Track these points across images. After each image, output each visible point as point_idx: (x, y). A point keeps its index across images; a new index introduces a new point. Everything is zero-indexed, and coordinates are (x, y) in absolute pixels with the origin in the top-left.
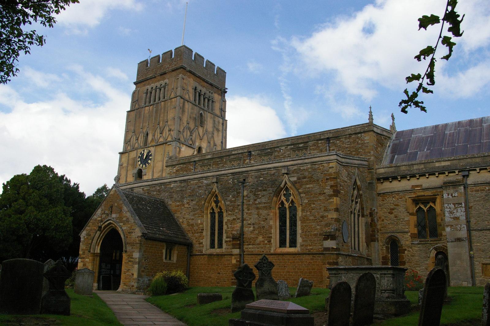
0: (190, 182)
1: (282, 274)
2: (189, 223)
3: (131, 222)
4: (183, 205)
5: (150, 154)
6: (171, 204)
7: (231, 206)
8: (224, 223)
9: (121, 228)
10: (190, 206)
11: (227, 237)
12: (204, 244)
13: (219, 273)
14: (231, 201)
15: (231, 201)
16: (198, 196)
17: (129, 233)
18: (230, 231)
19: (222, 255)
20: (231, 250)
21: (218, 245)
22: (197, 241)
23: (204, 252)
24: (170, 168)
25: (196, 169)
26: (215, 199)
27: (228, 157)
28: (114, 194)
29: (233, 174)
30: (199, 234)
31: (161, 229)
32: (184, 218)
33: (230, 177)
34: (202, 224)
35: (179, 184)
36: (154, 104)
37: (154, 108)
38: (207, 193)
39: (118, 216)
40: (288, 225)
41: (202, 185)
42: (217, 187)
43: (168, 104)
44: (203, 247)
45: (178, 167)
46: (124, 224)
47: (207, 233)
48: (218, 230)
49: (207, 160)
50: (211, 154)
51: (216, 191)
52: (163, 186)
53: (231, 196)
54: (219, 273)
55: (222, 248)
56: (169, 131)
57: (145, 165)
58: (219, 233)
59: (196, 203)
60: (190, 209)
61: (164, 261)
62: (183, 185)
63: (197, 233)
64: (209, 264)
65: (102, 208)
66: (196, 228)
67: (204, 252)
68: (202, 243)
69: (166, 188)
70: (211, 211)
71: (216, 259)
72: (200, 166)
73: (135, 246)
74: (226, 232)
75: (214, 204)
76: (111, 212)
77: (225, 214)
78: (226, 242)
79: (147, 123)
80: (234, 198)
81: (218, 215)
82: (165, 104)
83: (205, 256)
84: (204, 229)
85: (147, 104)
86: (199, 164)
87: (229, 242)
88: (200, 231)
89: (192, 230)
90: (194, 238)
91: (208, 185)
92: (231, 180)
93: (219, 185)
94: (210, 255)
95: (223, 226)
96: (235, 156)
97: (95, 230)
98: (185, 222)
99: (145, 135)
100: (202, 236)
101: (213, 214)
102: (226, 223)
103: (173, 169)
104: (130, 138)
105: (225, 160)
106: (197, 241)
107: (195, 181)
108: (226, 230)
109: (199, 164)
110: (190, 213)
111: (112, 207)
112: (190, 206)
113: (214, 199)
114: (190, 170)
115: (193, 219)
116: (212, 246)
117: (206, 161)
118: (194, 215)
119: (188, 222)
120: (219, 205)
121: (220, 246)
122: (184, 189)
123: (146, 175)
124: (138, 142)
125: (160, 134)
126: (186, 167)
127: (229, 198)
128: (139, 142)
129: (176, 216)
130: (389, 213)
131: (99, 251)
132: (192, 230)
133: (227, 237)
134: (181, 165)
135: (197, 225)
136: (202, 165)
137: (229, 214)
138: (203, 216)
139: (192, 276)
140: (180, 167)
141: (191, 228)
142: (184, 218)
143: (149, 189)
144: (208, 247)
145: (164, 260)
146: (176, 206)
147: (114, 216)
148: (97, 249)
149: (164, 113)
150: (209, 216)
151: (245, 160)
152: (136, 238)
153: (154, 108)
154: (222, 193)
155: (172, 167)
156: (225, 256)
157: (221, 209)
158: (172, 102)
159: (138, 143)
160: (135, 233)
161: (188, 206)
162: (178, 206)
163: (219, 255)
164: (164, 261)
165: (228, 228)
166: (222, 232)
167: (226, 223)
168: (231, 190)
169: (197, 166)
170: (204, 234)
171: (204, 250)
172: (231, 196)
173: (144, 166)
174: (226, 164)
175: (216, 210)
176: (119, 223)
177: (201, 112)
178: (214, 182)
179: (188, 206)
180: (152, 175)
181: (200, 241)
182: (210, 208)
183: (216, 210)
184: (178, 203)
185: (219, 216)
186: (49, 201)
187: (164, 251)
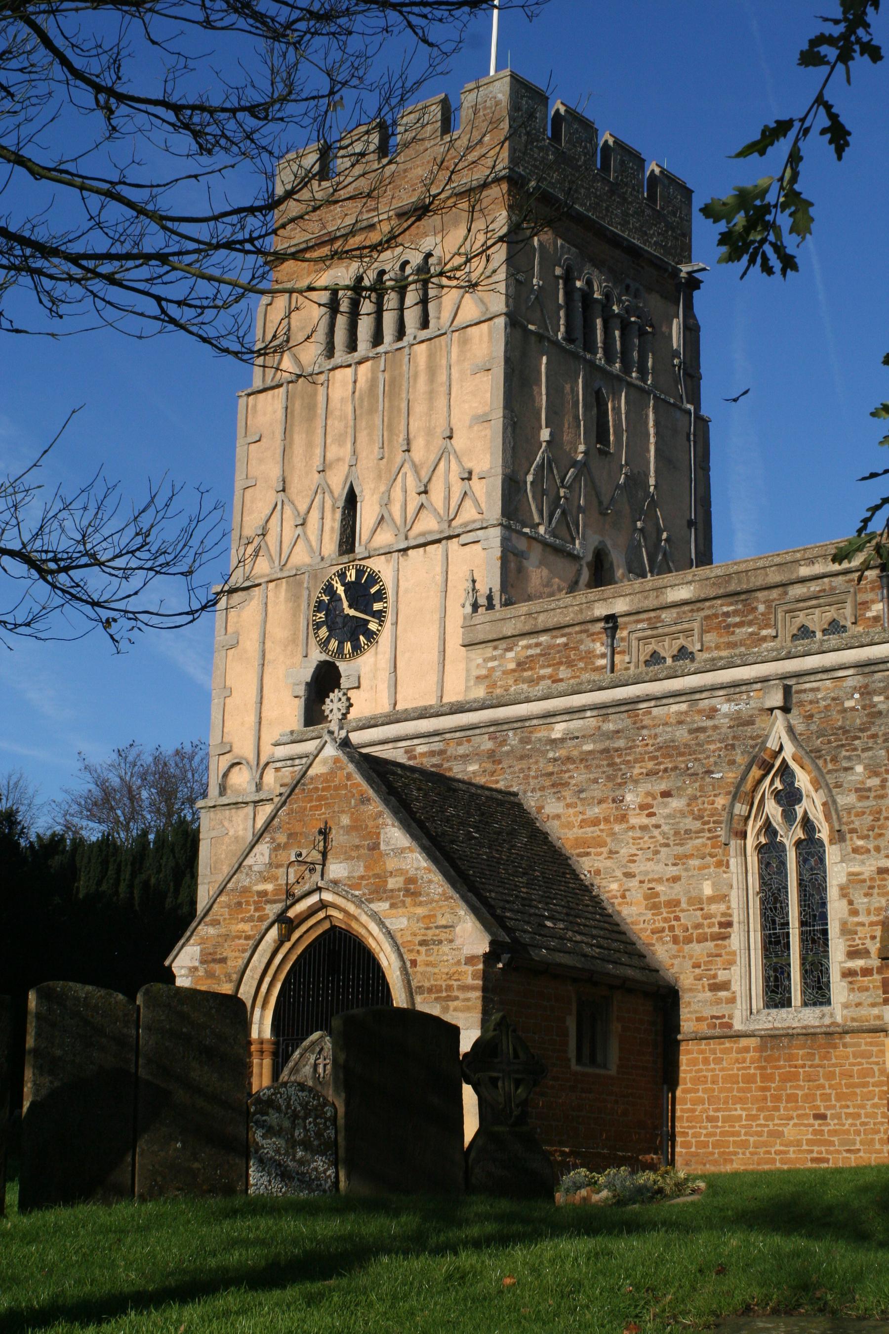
0: (650, 713)
2: (657, 895)
4: (623, 818)
5: (373, 591)
6: (558, 817)
8: (833, 893)
10: (653, 820)
11: (853, 954)
12: (735, 987)
13: (823, 1117)
14: (862, 792)
15: (862, 792)
17: (423, 943)
18: (862, 924)
19: (831, 1036)
20: (876, 1011)
21: (803, 993)
23: (738, 1026)
24: (489, 652)
25: (622, 652)
26: (778, 785)
27: (775, 594)
28: (332, 773)
29: (863, 666)
30: (710, 944)
32: (629, 875)
33: (850, 683)
34: (723, 898)
35: (593, 722)
36: (377, 357)
37: (381, 376)
38: (739, 759)
39: (361, 871)
40: (795, 984)
41: (710, 723)
42: (790, 730)
43: (449, 353)
44: (732, 1000)
45: (528, 647)
46: (393, 906)
47: (746, 942)
48: (803, 924)
49: (674, 611)
51: (781, 748)
52: (511, 734)
53: (859, 769)
54: (823, 1117)
55: (829, 1003)
58: (805, 938)
59: (689, 805)
60: (656, 832)
61: (574, 1067)
62: (610, 726)
63: (699, 942)
64: (765, 1078)
65: (273, 839)
66: (689, 917)
67: (738, 1026)
68: (725, 986)
69: (527, 743)
70: (763, 840)
71: (801, 1052)
72: (639, 640)
73: (456, 998)
74: (846, 931)
75: (773, 809)
76: (324, 854)
77: (832, 854)
78: (848, 974)
79: (349, 445)
81: (798, 855)
82: (431, 356)
83: (744, 1042)
84: (735, 919)
85: (340, 356)
86: (633, 627)
87: (864, 975)
88: (716, 929)
90: (688, 964)
91: (742, 722)
92: (857, 696)
95: (824, 904)
96: (814, 587)
97: (248, 938)
98: (637, 894)
100: (728, 954)
101: (770, 852)
102: (842, 888)
103: (502, 656)
104: (264, 517)
105: (761, 608)
106: (699, 978)
107: (674, 708)
108: (844, 924)
109: (633, 627)
110: (657, 852)
111: (324, 833)
112: (653, 820)
113: (772, 782)
115: (675, 879)
116: (776, 993)
117: (665, 615)
118: (680, 860)
121: (818, 992)
122: (621, 743)
123: (358, 687)
124: (305, 533)
125: (419, 494)
126: (566, 645)
127: (850, 779)
129: (586, 866)
130: (660, 1191)
131: (267, 1034)
132: (672, 929)
133: (853, 954)
134: (544, 638)
135: (697, 902)
136: (649, 633)
137: (856, 850)
138: (723, 864)
139: (685, 1134)
140: (537, 645)
141: (665, 920)
142: (629, 875)
143: (442, 752)
144: (758, 1002)
145: (573, 1061)
146: (583, 824)
147: (337, 869)
148: (261, 1023)
149: (431, 395)
150: (753, 860)
151: (866, 605)
152: (458, 963)
153: (381, 376)
154: (815, 754)
155: (495, 648)
156: (848, 1039)
158: (464, 342)
159: (308, 540)
160: (451, 941)
161: (646, 821)
162: (595, 822)
163: (814, 1034)
164: (574, 1067)
165: (854, 913)
166: (825, 932)
167: (842, 888)
168: (856, 742)
170: (736, 941)
171: (737, 1014)
172: (859, 769)
173: (348, 646)
175: (790, 836)
177: (596, 386)
178: (771, 710)
179: (646, 821)
180: (389, 687)
181: (715, 976)
182: (753, 826)
183: (790, 836)
184: (597, 810)
187: (571, 1024)
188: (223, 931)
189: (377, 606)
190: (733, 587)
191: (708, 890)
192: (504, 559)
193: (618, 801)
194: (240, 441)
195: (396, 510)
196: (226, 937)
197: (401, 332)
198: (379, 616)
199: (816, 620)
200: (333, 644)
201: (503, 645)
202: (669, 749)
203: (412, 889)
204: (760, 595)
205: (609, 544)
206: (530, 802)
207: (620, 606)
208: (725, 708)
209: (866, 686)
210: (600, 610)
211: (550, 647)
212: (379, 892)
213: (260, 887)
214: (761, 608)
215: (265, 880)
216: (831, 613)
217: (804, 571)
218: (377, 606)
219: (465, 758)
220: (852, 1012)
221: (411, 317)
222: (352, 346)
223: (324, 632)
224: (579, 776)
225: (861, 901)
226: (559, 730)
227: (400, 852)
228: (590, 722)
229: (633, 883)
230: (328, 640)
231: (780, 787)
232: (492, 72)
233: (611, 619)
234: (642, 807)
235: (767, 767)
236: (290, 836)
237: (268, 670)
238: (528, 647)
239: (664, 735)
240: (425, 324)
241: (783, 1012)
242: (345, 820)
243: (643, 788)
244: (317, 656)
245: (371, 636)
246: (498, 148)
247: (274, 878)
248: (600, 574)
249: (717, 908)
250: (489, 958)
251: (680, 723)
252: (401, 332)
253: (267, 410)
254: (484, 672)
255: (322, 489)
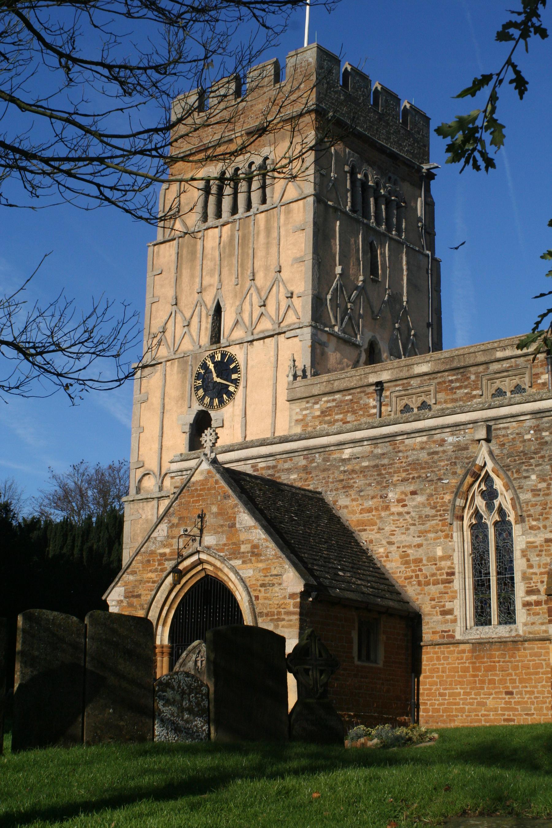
0: (404, 442)
1: (535, 701)
3: (266, 555)
4: (387, 508)
5: (231, 367)
6: (346, 507)
7: (536, 505)
9: (236, 573)
10: (406, 509)
11: (529, 592)
12: (457, 612)
13: (511, 693)
14: (535, 492)
15: (535, 492)
16: (430, 481)
17: (263, 585)
18: (535, 574)
19: (516, 643)
20: (544, 628)
21: (499, 616)
22: (434, 607)
23: (458, 637)
24: (304, 404)
25: (386, 405)
26: (483, 487)
27: (481, 368)
28: (206, 480)
29: (536, 414)
30: (441, 586)
31: (341, 573)
32: (390, 543)
33: (528, 424)
34: (449, 557)
35: (368, 448)
37: (236, 233)
38: (459, 471)
39: (224, 540)
42: (491, 453)
43: (279, 219)
44: (455, 621)
45: (328, 401)
46: (244, 562)
47: (463, 585)
48: (498, 573)
49: (419, 379)
50: (428, 362)
51: (485, 464)
52: (317, 455)
53: (534, 477)
54: (511, 693)
55: (515, 622)
56: (287, 297)
57: (212, 400)
58: (500, 582)
59: (428, 500)
61: (357, 662)
62: (379, 451)
63: (434, 584)
64: (475, 669)
66: (428, 569)
67: (458, 637)
68: (450, 612)
69: (327, 461)
70: (474, 521)
71: (497, 653)
72: (397, 397)
74: (526, 578)
75: (480, 502)
76: (201, 530)
77: (517, 530)
78: (527, 604)
79: (217, 276)
80: (544, 480)
81: (496, 531)
82: (268, 221)
83: (462, 647)
84: (457, 571)
85: (211, 221)
86: (393, 389)
87: (536, 605)
88: (445, 577)
89: (417, 576)
90: (428, 598)
91: (461, 448)
92: (532, 432)
93: (494, 446)
94: (479, 645)
95: (512, 561)
96: (506, 364)
98: (395, 555)
99: (212, 312)
100: (452, 592)
101: (478, 529)
102: (523, 551)
104: (164, 321)
105: (473, 377)
107: (419, 439)
108: (524, 574)
109: (393, 389)
110: (408, 529)
111: (201, 517)
112: (406, 509)
113: (479, 486)
114: (366, 407)
115: (419, 546)
116: (482, 616)
117: (413, 382)
119: (405, 555)
120: (496, 503)
121: (508, 615)
122: (385, 461)
123: (222, 427)
124: (189, 331)
125: (260, 306)
126: (351, 400)
127: (528, 483)
128: (195, 334)
129: (364, 537)
131: (166, 642)
133: (529, 592)
134: (337, 396)
135: (433, 560)
136: (403, 393)
137: (531, 528)
138: (449, 536)
140: (334, 400)
142: (390, 543)
143: (274, 467)
145: (356, 659)
146: (362, 511)
148: (162, 635)
149: (268, 245)
150: (467, 533)
151: (537, 375)
152: (285, 598)
153: (236, 233)
154: (506, 468)
155: (308, 402)
156: (526, 645)
157: (501, 512)
159: (191, 335)
160: (280, 584)
161: (401, 509)
162: (370, 510)
163: (506, 642)
164: (357, 662)
165: (531, 566)
166: (512, 579)
167: (523, 551)
168: (532, 461)
169: (386, 397)
170: (457, 584)
171: (458, 629)
172: (534, 477)
173: (216, 401)
174: (476, 389)
176: (230, 559)
177: (370, 240)
178: (479, 441)
179: (401, 509)
180: (241, 427)
181: (444, 606)
182: (468, 513)
183: (490, 519)
184: (370, 503)
185: (498, 534)
186: (539, 444)
187: (355, 635)
188: (138, 578)
189: (234, 376)
190: (455, 364)
191: (439, 552)
192: (313, 347)
193: (384, 497)
194: (149, 274)
195: (246, 316)
196: (141, 581)
197: (249, 206)
198: (236, 382)
199: (507, 385)
200: (207, 400)
201: (312, 400)
202: (415, 465)
203: (256, 552)
204: (472, 369)
205: (378, 337)
206: (329, 498)
207: (385, 376)
208: (450, 439)
209: (538, 426)
210: (373, 379)
211: (341, 401)
212: (235, 553)
213: (162, 551)
214: (473, 377)
215: (165, 546)
216: (516, 381)
217: (500, 354)
218: (234, 376)
219: (289, 470)
220: (529, 628)
221: (256, 197)
222: (219, 215)
223: (201, 392)
224: (360, 482)
225: (534, 559)
226: (347, 453)
227: (248, 529)
228: (366, 448)
229: (393, 548)
230: (204, 397)
231: (484, 489)
232: (306, 45)
233: (379, 384)
234: (399, 501)
235: (476, 476)
236: (180, 519)
237: (166, 416)
238: (328, 401)
239: (412, 456)
240: (264, 201)
241: (486, 628)
242: (214, 509)
243: (399, 489)
244: (197, 407)
245: (230, 395)
246: (309, 92)
247: (170, 545)
248: (373, 356)
249: (445, 564)
250: (304, 595)
251: (422, 448)
252: (249, 206)
253: (166, 255)
254: (300, 417)
255: (200, 303)
